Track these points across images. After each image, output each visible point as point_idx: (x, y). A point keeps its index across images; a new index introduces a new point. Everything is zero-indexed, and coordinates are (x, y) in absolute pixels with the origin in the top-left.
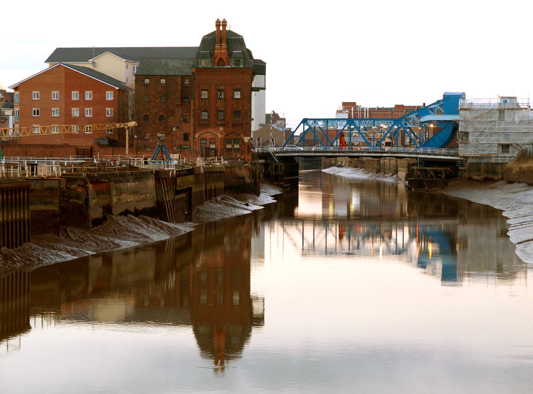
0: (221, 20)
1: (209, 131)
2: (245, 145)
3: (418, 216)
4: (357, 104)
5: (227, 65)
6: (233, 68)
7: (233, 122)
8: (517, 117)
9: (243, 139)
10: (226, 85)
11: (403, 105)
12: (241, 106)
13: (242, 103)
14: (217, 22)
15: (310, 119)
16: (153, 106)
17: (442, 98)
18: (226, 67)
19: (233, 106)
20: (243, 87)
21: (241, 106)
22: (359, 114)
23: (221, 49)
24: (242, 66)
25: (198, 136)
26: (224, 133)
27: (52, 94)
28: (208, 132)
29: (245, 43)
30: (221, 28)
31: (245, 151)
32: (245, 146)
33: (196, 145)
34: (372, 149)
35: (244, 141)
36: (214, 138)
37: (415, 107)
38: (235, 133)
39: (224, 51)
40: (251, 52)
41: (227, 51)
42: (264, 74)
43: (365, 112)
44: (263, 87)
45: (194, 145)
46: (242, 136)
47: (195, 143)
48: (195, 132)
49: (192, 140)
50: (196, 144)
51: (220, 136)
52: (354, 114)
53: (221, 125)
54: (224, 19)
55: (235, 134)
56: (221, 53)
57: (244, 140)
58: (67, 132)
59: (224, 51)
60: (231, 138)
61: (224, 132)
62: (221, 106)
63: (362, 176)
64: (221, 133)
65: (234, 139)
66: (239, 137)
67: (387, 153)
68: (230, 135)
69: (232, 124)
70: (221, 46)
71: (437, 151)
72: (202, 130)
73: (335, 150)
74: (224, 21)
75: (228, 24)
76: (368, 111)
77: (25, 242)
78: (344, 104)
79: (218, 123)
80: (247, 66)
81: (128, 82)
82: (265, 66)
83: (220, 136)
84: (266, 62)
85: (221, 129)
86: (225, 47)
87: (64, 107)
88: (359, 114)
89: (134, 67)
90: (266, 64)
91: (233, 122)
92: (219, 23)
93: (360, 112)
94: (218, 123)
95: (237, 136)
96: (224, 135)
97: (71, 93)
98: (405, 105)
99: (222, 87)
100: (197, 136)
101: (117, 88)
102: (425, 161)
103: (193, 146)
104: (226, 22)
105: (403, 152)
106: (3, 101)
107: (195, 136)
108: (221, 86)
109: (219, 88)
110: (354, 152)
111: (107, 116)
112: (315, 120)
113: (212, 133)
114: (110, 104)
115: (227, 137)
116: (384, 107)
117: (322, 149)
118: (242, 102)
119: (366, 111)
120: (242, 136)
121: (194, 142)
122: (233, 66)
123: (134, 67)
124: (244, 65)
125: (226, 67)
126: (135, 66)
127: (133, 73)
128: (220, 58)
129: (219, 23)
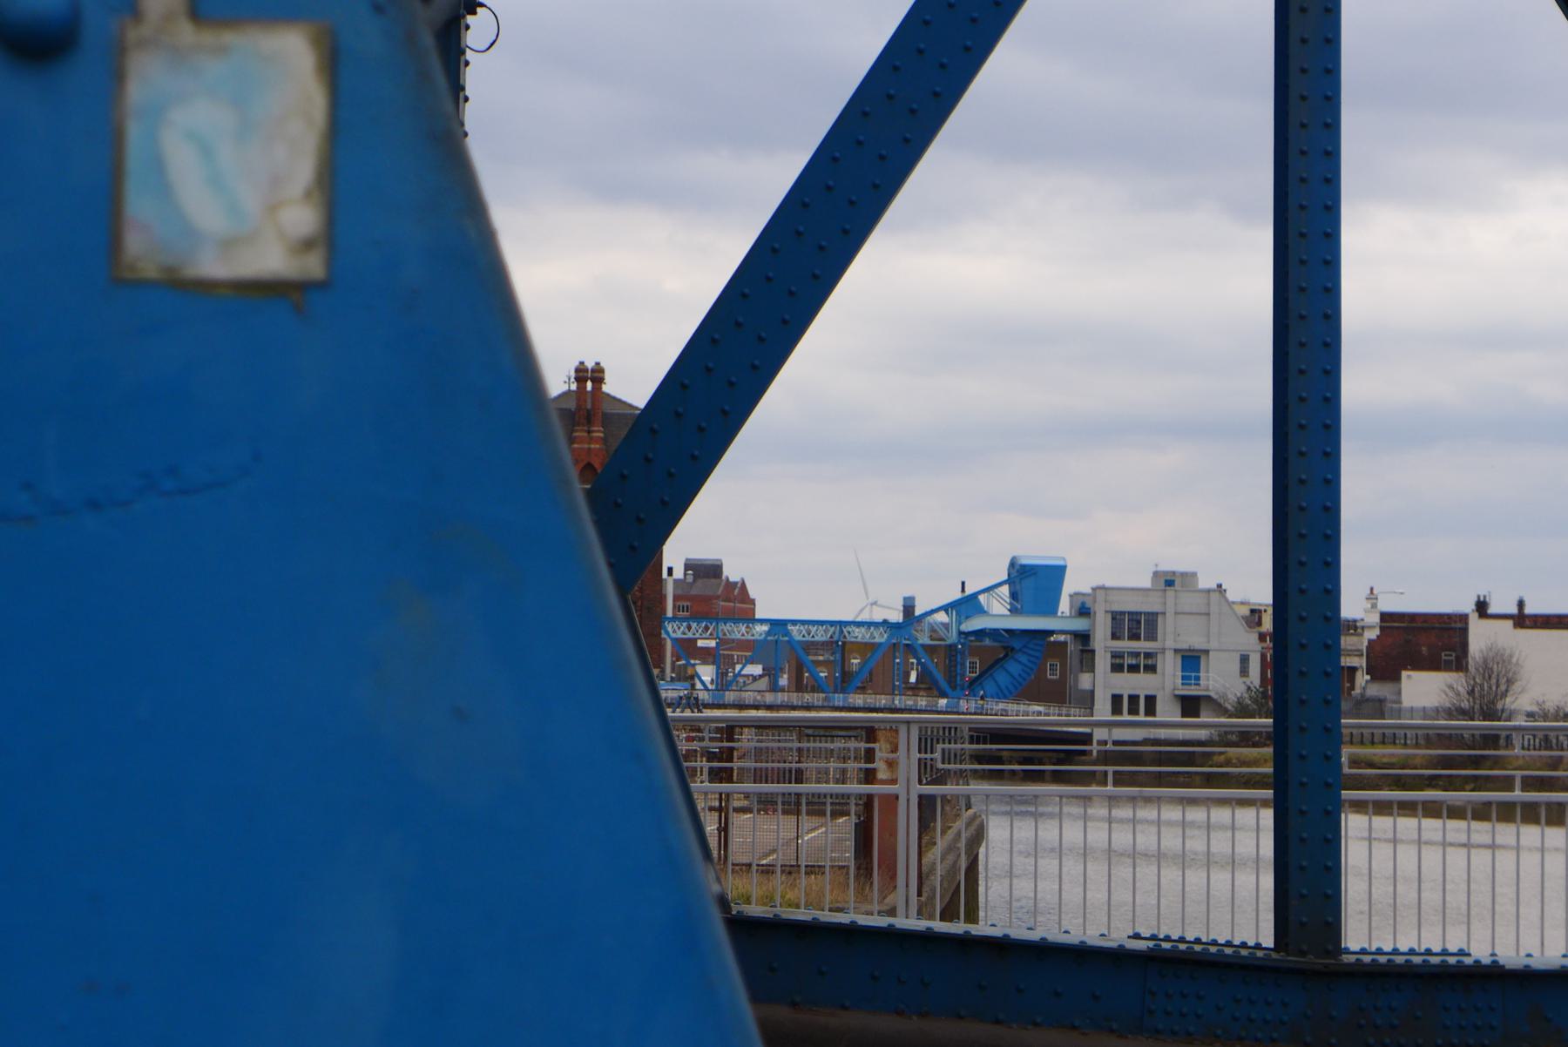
0: (590, 365)
3: (828, 887)
8: (612, 560)
14: (577, 370)
15: (794, 622)
23: (591, 440)
30: (589, 385)
39: (598, 446)
41: (604, 447)
54: (598, 364)
56: (589, 449)
59: (598, 446)
70: (589, 432)
71: (1012, 707)
73: (816, 703)
74: (582, 367)
75: (608, 377)
86: (596, 429)
92: (585, 374)
102: (991, 735)
104: (602, 371)
105: (819, 707)
117: (883, 701)
128: (585, 462)
129: (585, 374)
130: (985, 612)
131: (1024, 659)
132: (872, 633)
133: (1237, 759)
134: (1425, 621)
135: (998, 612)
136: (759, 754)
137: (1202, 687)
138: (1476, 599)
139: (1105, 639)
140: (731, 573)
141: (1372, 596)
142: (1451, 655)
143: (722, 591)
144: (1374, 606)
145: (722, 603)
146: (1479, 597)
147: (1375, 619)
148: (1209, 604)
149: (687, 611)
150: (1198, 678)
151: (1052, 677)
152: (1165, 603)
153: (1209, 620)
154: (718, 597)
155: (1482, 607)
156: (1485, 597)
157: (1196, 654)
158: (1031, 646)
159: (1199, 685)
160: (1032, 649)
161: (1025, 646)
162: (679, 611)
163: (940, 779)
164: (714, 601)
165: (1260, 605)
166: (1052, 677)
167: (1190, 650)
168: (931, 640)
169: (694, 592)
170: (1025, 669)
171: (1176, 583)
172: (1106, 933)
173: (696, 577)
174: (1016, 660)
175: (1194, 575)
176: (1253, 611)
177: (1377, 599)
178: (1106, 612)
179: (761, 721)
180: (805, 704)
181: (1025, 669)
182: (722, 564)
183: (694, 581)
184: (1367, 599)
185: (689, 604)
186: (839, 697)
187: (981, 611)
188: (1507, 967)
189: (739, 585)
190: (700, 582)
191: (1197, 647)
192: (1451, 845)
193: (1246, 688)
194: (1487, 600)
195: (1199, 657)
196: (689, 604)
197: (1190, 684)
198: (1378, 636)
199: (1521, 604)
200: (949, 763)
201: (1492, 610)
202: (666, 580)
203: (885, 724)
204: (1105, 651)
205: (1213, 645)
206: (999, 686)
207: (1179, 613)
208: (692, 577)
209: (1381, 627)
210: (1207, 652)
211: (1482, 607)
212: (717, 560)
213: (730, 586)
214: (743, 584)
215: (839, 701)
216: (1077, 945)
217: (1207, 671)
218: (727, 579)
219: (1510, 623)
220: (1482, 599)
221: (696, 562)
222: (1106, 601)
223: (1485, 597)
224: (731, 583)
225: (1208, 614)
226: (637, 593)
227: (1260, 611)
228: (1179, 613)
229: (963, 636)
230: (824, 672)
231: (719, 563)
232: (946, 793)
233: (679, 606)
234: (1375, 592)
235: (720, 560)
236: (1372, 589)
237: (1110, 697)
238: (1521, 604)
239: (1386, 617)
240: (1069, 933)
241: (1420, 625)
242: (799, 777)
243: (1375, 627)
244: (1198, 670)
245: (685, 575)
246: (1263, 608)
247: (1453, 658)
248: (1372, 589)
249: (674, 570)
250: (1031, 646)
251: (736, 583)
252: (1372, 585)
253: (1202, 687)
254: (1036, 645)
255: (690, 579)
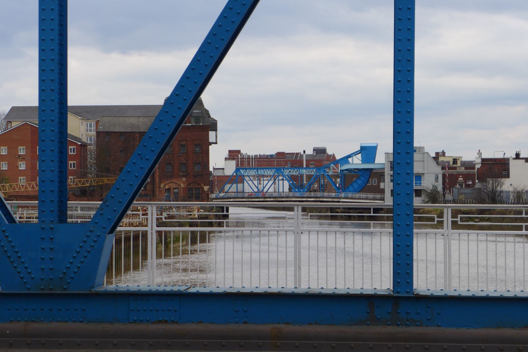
1: (173, 181)
2: (205, 193)
4: (241, 152)
5: (188, 123)
6: (193, 126)
7: (194, 173)
9: (203, 187)
10: (187, 140)
11: (284, 152)
12: (200, 159)
13: (202, 156)
16: (114, 159)
17: (360, 149)
18: (187, 125)
19: (194, 159)
20: (202, 142)
21: (200, 159)
22: (246, 161)
24: (201, 124)
25: (164, 186)
26: (186, 183)
27: (75, 152)
28: (172, 182)
29: (203, 104)
31: (205, 198)
32: (205, 194)
33: (161, 194)
34: (299, 195)
35: (204, 190)
36: (178, 187)
37: (293, 154)
38: (195, 183)
40: (209, 111)
42: (216, 130)
43: (251, 159)
44: (215, 141)
45: (160, 194)
46: (202, 185)
47: (160, 192)
48: (160, 183)
49: (158, 189)
50: (161, 193)
51: (182, 186)
52: (240, 161)
53: (184, 176)
55: (195, 184)
57: (204, 189)
58: (80, 186)
60: (192, 187)
61: (186, 182)
62: (183, 159)
63: (464, 209)
64: (184, 183)
65: (195, 188)
66: (200, 187)
67: (313, 198)
68: (192, 184)
69: (193, 175)
72: (167, 180)
76: (253, 158)
77: (127, 269)
78: (230, 152)
79: (181, 174)
80: (206, 124)
81: (83, 137)
82: (216, 124)
83: (182, 186)
84: (217, 120)
85: (184, 179)
87: (30, 161)
88: (246, 161)
89: (87, 124)
90: (218, 122)
91: (194, 173)
93: (246, 159)
94: (181, 174)
95: (198, 185)
96: (186, 185)
97: (18, 148)
98: (286, 152)
99: (184, 143)
100: (162, 186)
101: (79, 143)
103: (159, 195)
105: (326, 197)
106: (20, 158)
107: (160, 186)
108: (183, 142)
109: (182, 144)
110: (333, 197)
111: (70, 169)
112: (435, 178)
113: (175, 183)
114: (73, 158)
115: (189, 187)
116: (265, 154)
118: (201, 156)
119: (252, 158)
120: (202, 185)
121: (160, 191)
122: (194, 124)
123: (87, 124)
124: (203, 124)
125: (187, 125)
126: (89, 123)
127: (87, 129)
130: (349, 163)
131: (362, 178)
132: (308, 171)
133: (427, 210)
134: (500, 161)
135: (357, 162)
136: (200, 217)
137: (422, 186)
138: (516, 153)
139: (388, 171)
140: (329, 152)
141: (479, 153)
142: (506, 173)
143: (326, 158)
144: (480, 156)
145: (325, 162)
146: (517, 152)
147: (479, 161)
148: (424, 158)
149: (314, 165)
150: (421, 183)
151: (374, 184)
152: (424, 158)
153: (424, 162)
154: (324, 160)
155: (518, 156)
156: (519, 152)
157: (421, 175)
158: (365, 174)
159: (421, 185)
160: (365, 175)
161: (362, 174)
162: (311, 165)
163: (165, 224)
164: (323, 161)
165: (457, 157)
166: (374, 184)
167: (417, 174)
168: (333, 173)
169: (316, 159)
170: (363, 182)
171: (417, 151)
172: (258, 286)
173: (317, 153)
174: (360, 179)
175: (423, 148)
176: (454, 159)
177: (481, 154)
178: (388, 161)
179: (235, 207)
180: (286, 196)
181: (363, 182)
182: (326, 149)
183: (316, 155)
184: (478, 154)
185: (314, 162)
186: (291, 193)
187: (348, 163)
188: (309, 292)
189: (332, 156)
190: (318, 155)
191: (420, 172)
192: (489, 241)
193: (432, 186)
194: (520, 153)
195: (421, 176)
196: (314, 162)
197: (417, 185)
198: (480, 167)
199: (480, 153)
200: (75, 219)
201: (521, 157)
202: (303, 155)
203: (90, 205)
204: (388, 175)
205: (425, 172)
206: (354, 189)
207: (423, 161)
208: (315, 153)
209: (481, 164)
210: (423, 174)
211: (518, 156)
212: (324, 147)
213: (329, 156)
214: (334, 155)
215: (298, 195)
216: (196, 292)
217: (424, 181)
218: (328, 154)
219: (524, 161)
220: (518, 153)
221: (317, 148)
222: (388, 158)
223: (519, 152)
224: (329, 155)
225: (424, 161)
226: (201, 161)
227: (457, 159)
228: (423, 161)
229: (342, 171)
230: (316, 185)
231: (325, 148)
232: (222, 230)
233: (311, 164)
234: (481, 152)
235: (325, 147)
236: (479, 150)
237: (390, 190)
238: (480, 153)
239: (483, 160)
240: (271, 288)
241: (498, 162)
242: (284, 227)
243: (479, 163)
244: (421, 181)
245: (313, 153)
246: (458, 158)
247: (507, 173)
248: (479, 150)
249: (306, 151)
250: (365, 174)
251: (331, 155)
252: (479, 149)
253: (422, 186)
254: (366, 173)
255: (315, 154)
